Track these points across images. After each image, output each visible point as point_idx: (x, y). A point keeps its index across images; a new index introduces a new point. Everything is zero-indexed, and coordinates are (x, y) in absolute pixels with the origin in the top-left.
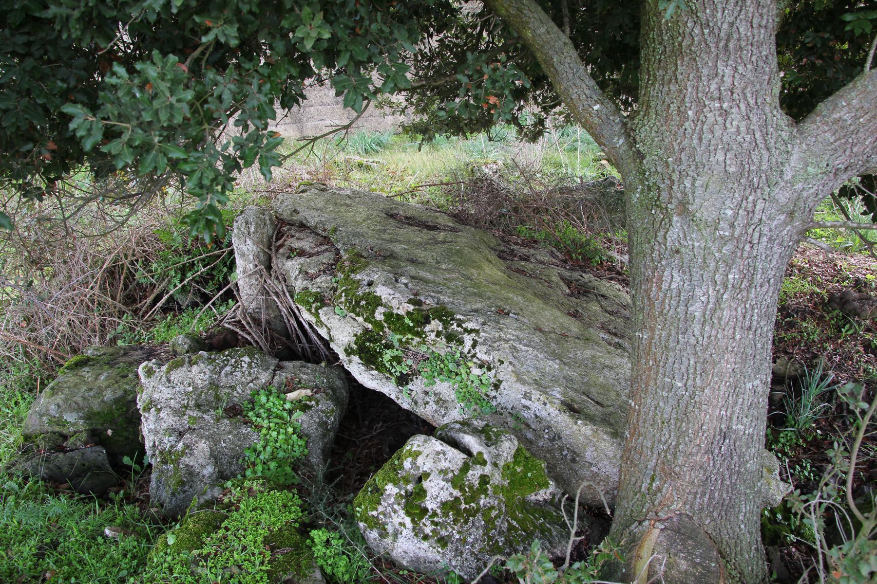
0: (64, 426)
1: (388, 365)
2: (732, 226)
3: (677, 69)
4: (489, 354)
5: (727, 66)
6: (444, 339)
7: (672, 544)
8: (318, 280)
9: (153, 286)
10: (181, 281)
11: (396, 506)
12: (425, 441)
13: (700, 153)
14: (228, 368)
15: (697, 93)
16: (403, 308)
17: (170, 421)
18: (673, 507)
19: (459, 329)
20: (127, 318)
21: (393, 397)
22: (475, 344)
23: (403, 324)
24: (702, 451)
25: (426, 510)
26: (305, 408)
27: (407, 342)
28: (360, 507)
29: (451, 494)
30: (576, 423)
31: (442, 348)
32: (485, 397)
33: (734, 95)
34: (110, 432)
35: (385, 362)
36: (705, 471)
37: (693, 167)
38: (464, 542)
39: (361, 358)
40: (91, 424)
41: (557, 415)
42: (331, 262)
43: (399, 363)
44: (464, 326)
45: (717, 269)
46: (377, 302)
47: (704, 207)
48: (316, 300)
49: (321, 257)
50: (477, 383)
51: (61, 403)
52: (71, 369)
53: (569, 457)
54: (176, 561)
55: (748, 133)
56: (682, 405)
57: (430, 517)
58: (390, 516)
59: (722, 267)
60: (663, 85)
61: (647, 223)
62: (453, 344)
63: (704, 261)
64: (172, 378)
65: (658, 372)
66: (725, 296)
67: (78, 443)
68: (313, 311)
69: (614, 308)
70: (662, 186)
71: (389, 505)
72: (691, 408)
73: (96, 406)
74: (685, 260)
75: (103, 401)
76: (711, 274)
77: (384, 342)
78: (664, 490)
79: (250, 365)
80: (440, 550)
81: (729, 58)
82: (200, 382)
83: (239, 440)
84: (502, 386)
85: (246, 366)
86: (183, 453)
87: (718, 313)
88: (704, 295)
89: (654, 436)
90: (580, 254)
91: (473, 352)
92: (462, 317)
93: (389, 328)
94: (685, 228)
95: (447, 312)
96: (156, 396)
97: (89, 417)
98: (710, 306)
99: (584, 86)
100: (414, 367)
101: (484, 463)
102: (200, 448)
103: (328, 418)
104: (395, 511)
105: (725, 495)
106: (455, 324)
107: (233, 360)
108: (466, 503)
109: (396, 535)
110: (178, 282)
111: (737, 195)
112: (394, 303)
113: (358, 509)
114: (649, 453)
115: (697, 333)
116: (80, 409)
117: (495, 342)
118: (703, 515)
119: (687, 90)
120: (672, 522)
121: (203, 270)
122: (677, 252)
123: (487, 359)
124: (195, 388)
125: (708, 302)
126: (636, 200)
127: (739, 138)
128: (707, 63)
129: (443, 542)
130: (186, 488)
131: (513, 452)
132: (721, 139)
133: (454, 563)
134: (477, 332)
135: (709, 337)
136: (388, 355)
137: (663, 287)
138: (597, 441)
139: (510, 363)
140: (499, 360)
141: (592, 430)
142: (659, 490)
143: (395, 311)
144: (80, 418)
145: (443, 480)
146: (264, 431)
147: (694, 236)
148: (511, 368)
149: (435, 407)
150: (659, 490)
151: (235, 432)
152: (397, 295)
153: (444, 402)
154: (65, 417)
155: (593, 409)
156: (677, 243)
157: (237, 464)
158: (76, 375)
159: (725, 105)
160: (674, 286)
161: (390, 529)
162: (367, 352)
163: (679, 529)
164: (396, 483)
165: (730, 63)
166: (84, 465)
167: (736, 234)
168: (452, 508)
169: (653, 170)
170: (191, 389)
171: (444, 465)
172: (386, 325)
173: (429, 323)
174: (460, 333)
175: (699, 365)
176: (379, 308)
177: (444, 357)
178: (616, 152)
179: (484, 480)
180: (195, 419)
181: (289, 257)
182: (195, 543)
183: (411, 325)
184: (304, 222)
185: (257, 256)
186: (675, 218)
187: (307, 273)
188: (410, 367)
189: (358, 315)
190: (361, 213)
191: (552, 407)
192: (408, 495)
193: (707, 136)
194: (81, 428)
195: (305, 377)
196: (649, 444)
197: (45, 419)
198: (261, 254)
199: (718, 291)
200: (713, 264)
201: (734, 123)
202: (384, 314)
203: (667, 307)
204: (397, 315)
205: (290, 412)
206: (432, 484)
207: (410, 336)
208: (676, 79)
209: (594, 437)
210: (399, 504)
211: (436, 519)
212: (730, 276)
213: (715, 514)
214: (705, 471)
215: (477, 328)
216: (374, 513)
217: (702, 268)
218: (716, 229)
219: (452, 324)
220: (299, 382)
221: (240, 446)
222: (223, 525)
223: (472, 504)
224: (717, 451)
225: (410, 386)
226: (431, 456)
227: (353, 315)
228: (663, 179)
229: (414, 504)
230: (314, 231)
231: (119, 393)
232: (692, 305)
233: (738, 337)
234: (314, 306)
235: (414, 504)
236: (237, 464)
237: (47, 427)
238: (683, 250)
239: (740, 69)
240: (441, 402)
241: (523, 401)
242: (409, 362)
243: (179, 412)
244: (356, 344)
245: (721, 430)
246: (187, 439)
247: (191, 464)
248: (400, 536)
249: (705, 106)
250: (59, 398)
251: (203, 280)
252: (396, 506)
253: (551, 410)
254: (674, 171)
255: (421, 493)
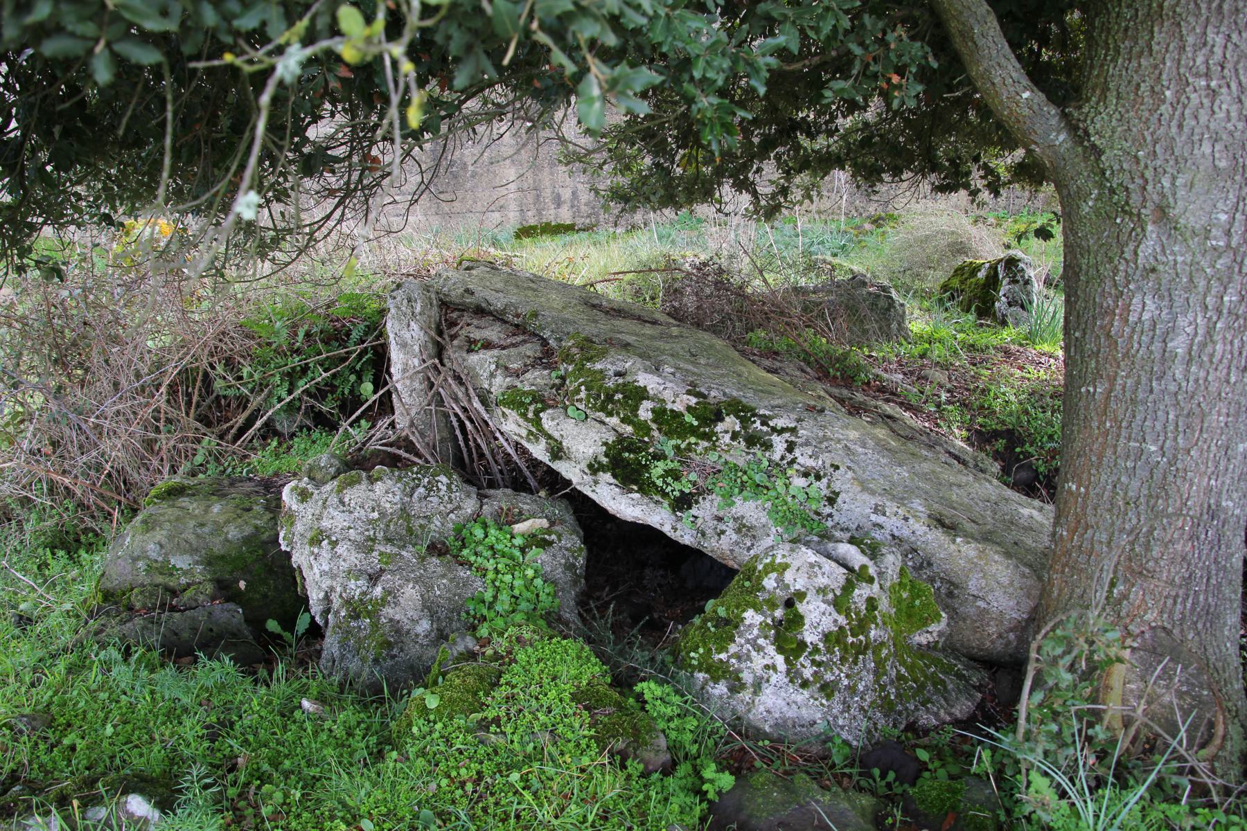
0: (172, 575)
1: (659, 483)
2: (1228, 233)
3: (1152, 37)
4: (817, 458)
5: (1218, 33)
6: (743, 443)
7: (1147, 670)
8: (528, 375)
9: (243, 402)
10: (290, 392)
11: (761, 641)
12: (792, 550)
13: (1180, 144)
14: (421, 490)
15: (1178, 68)
16: (680, 402)
17: (353, 558)
18: (1148, 617)
19: (765, 428)
20: (210, 441)
21: (667, 529)
22: (790, 447)
23: (682, 423)
24: (1185, 537)
25: (802, 645)
26: (545, 544)
27: (689, 448)
28: (696, 650)
29: (835, 621)
30: (954, 542)
31: (739, 455)
32: (815, 517)
33: (1226, 71)
34: (242, 584)
35: (654, 479)
36: (1189, 564)
37: (1172, 163)
38: (852, 689)
39: (614, 476)
40: (215, 573)
41: (926, 533)
42: (539, 354)
43: (677, 478)
44: (771, 424)
45: (1208, 289)
46: (641, 394)
47: (1191, 210)
48: (534, 401)
49: (522, 349)
50: (801, 497)
51: (164, 541)
52: (163, 499)
53: (943, 591)
54: (450, 729)
55: (1240, 120)
56: (1158, 475)
57: (810, 653)
58: (749, 658)
59: (1216, 287)
60: (1130, 60)
61: (1108, 236)
62: (756, 449)
63: (1191, 280)
64: (346, 500)
65: (1119, 436)
66: (1219, 325)
67: (201, 598)
68: (530, 415)
69: (908, 433)
70: (1131, 186)
71: (748, 641)
72: (1170, 478)
73: (218, 549)
74: (1164, 281)
75: (227, 540)
76: (1200, 297)
77: (651, 450)
78: (1132, 596)
79: (449, 487)
80: (824, 701)
81: (1221, 21)
82: (388, 505)
83: (457, 586)
84: (839, 500)
85: (444, 488)
86: (383, 602)
87: (1209, 349)
88: (1189, 325)
89: (1113, 524)
90: (837, 370)
91: (789, 457)
92: (767, 413)
93: (660, 430)
94: (1164, 239)
95: (744, 406)
96: (325, 524)
97: (211, 561)
98: (1199, 338)
99: (1010, 67)
100: (700, 482)
101: (871, 580)
102: (407, 595)
103: (576, 559)
104: (759, 649)
105: (1210, 600)
106: (758, 422)
107: (426, 480)
108: (852, 636)
109: (757, 687)
110: (284, 394)
111: (1231, 196)
112: (668, 395)
113: (692, 654)
114: (1105, 549)
115: (1178, 376)
116: (193, 551)
117: (821, 443)
118: (1185, 627)
119: (1164, 64)
120: (1144, 640)
121: (324, 375)
122: (1153, 270)
123: (814, 464)
124: (383, 514)
125: (1196, 334)
126: (1087, 209)
127: (1230, 126)
128: (1194, 28)
129: (827, 689)
130: (395, 651)
131: (898, 570)
132: (1208, 127)
133: (841, 722)
134: (793, 431)
135: (1197, 381)
136: (658, 469)
137: (1130, 319)
138: (986, 564)
139: (849, 468)
140: (832, 465)
141: (978, 549)
142: (1125, 597)
143: (669, 406)
144: (197, 563)
145: (823, 601)
146: (491, 575)
147: (1176, 249)
148: (850, 474)
149: (734, 537)
150: (1125, 597)
151: (450, 576)
152: (669, 385)
153: (749, 529)
154: (173, 561)
155: (969, 526)
156: (1151, 259)
157: (459, 620)
158: (173, 506)
159: (1213, 84)
160: (1146, 316)
161: (747, 677)
162: (625, 467)
163: (1155, 648)
164: (758, 609)
165: (1223, 29)
166: (211, 630)
167: (1234, 244)
168: (838, 642)
169: (1116, 167)
170: (376, 515)
171: (822, 581)
172: (654, 426)
173: (722, 420)
174: (767, 433)
175: (1181, 419)
176: (645, 402)
177: (745, 467)
178: (1055, 153)
179: (871, 603)
180: (390, 556)
181: (470, 351)
182: (471, 704)
183: (696, 423)
184: (484, 305)
185: (424, 347)
186: (1150, 228)
187: (507, 368)
188: (694, 484)
189: (610, 414)
190: (556, 300)
191: (918, 522)
192: (778, 624)
193: (1189, 122)
194: (199, 578)
195: (525, 507)
196: (1104, 537)
197: (140, 564)
198: (430, 345)
199: (1210, 319)
200: (1202, 284)
201: (1224, 107)
202: (653, 411)
203: (1136, 346)
204: (672, 411)
205: (523, 550)
206: (811, 607)
207: (693, 440)
208: (1151, 50)
209: (981, 558)
210: (766, 637)
211: (817, 658)
212: (1226, 299)
213: (1200, 626)
214: (1189, 564)
215: (793, 425)
216: (723, 656)
217: (1187, 290)
218: (1207, 238)
219: (754, 422)
220: (521, 513)
221: (459, 595)
222: (502, 681)
223: (861, 637)
224: (1203, 536)
225: (694, 511)
226: (804, 569)
227: (601, 415)
228: (1133, 179)
229: (786, 634)
230: (498, 317)
231: (248, 530)
232: (1172, 340)
233: (1233, 379)
234: (532, 408)
235: (786, 634)
236: (459, 620)
237: (142, 577)
238: (1161, 268)
239: (1235, 37)
240: (743, 528)
241: (873, 517)
242: (693, 476)
243: (366, 546)
244: (606, 455)
245: (1209, 506)
246: (387, 581)
247: (397, 617)
248: (765, 685)
249: (1188, 84)
250: (160, 535)
251: (320, 393)
252: (761, 641)
253: (917, 526)
254: (1146, 167)
255: (796, 621)
